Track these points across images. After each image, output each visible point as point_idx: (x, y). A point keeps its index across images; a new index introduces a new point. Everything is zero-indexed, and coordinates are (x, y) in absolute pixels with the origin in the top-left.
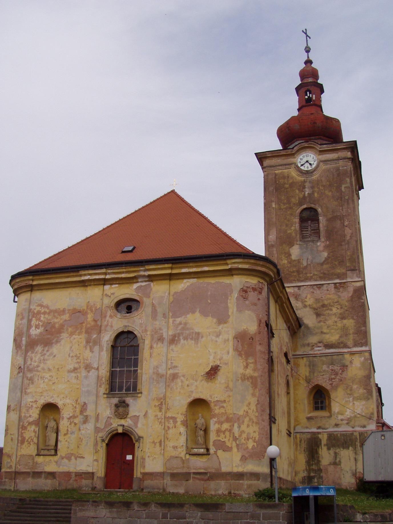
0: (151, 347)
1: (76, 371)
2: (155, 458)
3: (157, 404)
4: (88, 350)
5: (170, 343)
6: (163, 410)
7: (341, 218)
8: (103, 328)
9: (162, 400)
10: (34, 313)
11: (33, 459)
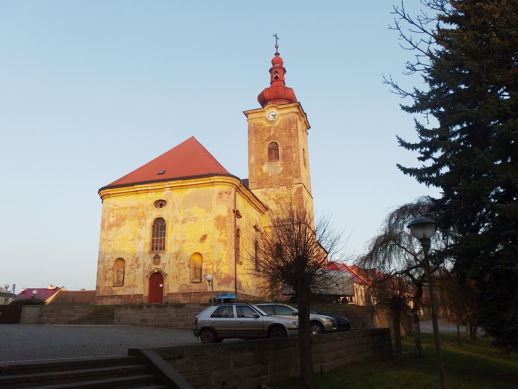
0: (172, 226)
4: (139, 229)
7: (291, 148)
8: (147, 216)
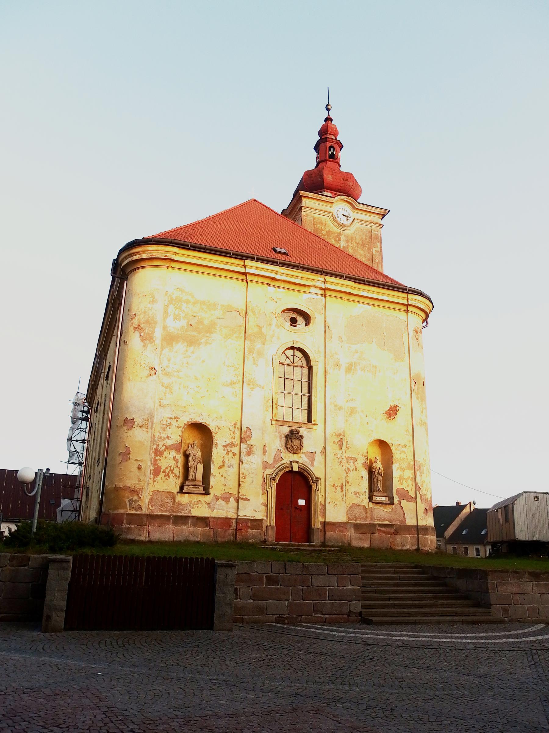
1: (233, 386)
2: (336, 505)
3: (336, 441)
5: (346, 372)
6: (344, 448)
9: (341, 437)
10: (172, 299)
11: (174, 498)
